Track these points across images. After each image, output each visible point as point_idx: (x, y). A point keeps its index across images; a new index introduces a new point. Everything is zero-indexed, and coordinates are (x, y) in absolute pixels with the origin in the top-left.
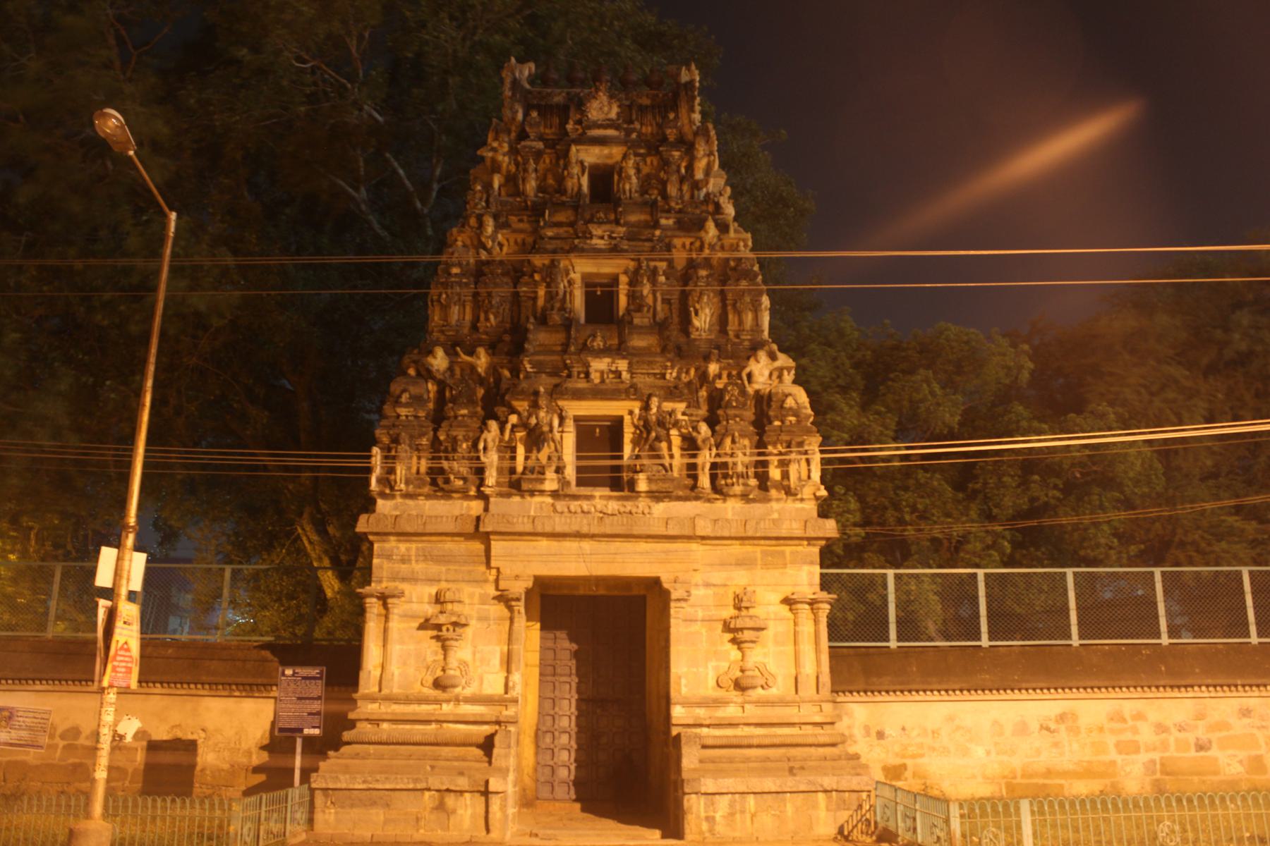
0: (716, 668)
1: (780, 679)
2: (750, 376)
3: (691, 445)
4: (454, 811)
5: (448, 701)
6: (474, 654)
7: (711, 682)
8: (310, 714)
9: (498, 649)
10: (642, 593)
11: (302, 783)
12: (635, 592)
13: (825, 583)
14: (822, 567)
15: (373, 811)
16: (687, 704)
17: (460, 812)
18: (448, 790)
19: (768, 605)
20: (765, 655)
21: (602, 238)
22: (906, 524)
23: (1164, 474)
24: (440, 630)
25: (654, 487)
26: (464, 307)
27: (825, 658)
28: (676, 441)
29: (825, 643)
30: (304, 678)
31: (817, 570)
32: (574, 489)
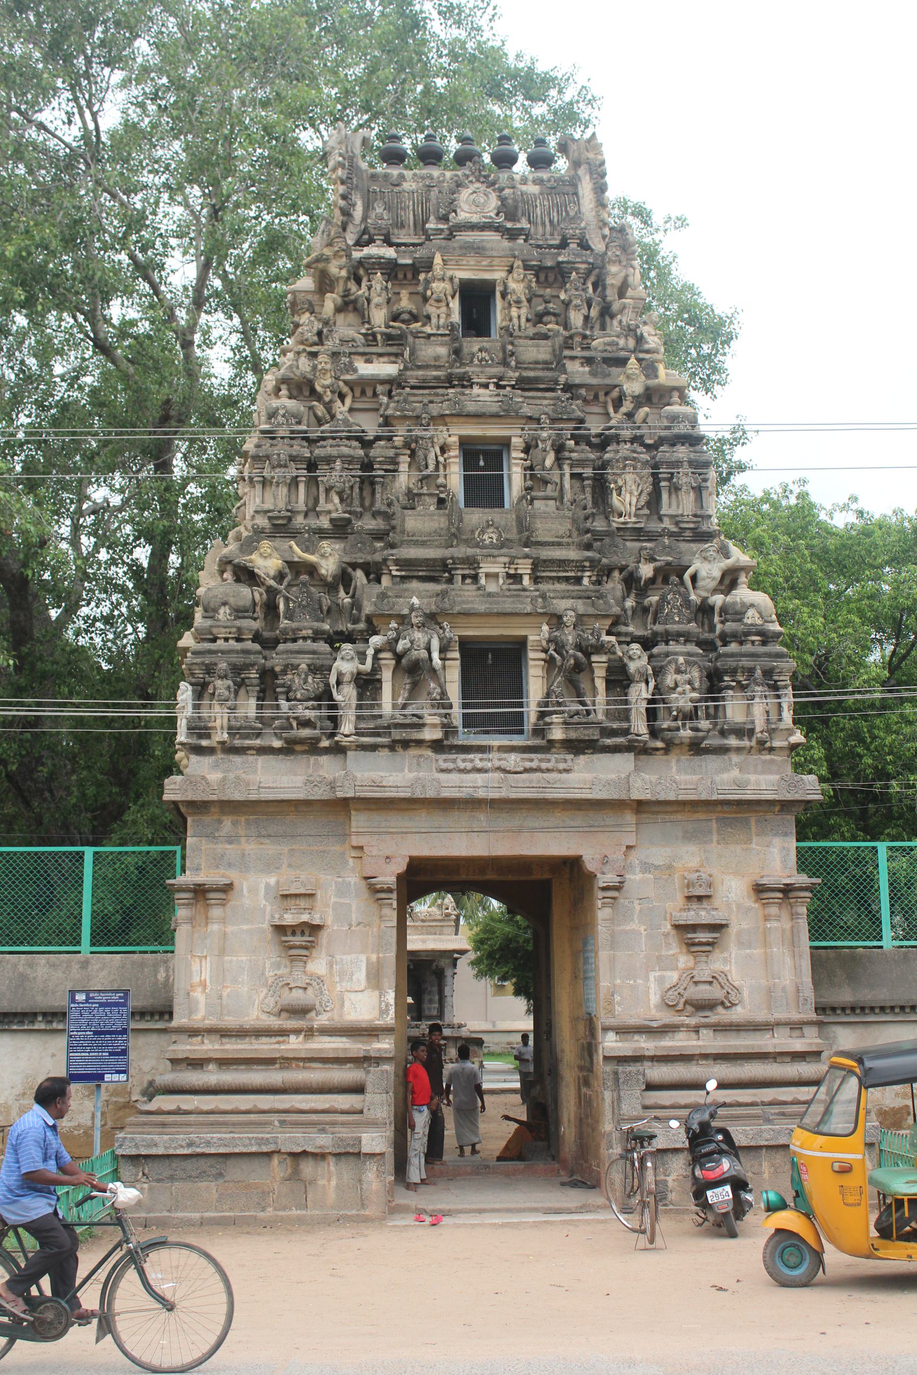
0: (660, 980)
1: (745, 993)
2: (694, 578)
3: (619, 679)
4: (313, 1182)
5: (297, 1032)
6: (331, 965)
7: (654, 998)
8: (111, 1054)
9: (363, 958)
10: (546, 876)
11: (103, 1148)
12: (537, 876)
13: (804, 862)
14: (798, 840)
15: (203, 1184)
16: (624, 1031)
17: (321, 1182)
18: (305, 1153)
19: (732, 893)
20: (726, 961)
21: (486, 386)
22: (889, 777)
23: (622, 230)
24: (297, 937)
25: (573, 735)
26: (542, 577)
27: (806, 964)
28: (600, 673)
29: (805, 943)
30: (101, 1005)
31: (792, 843)
32: (464, 738)
